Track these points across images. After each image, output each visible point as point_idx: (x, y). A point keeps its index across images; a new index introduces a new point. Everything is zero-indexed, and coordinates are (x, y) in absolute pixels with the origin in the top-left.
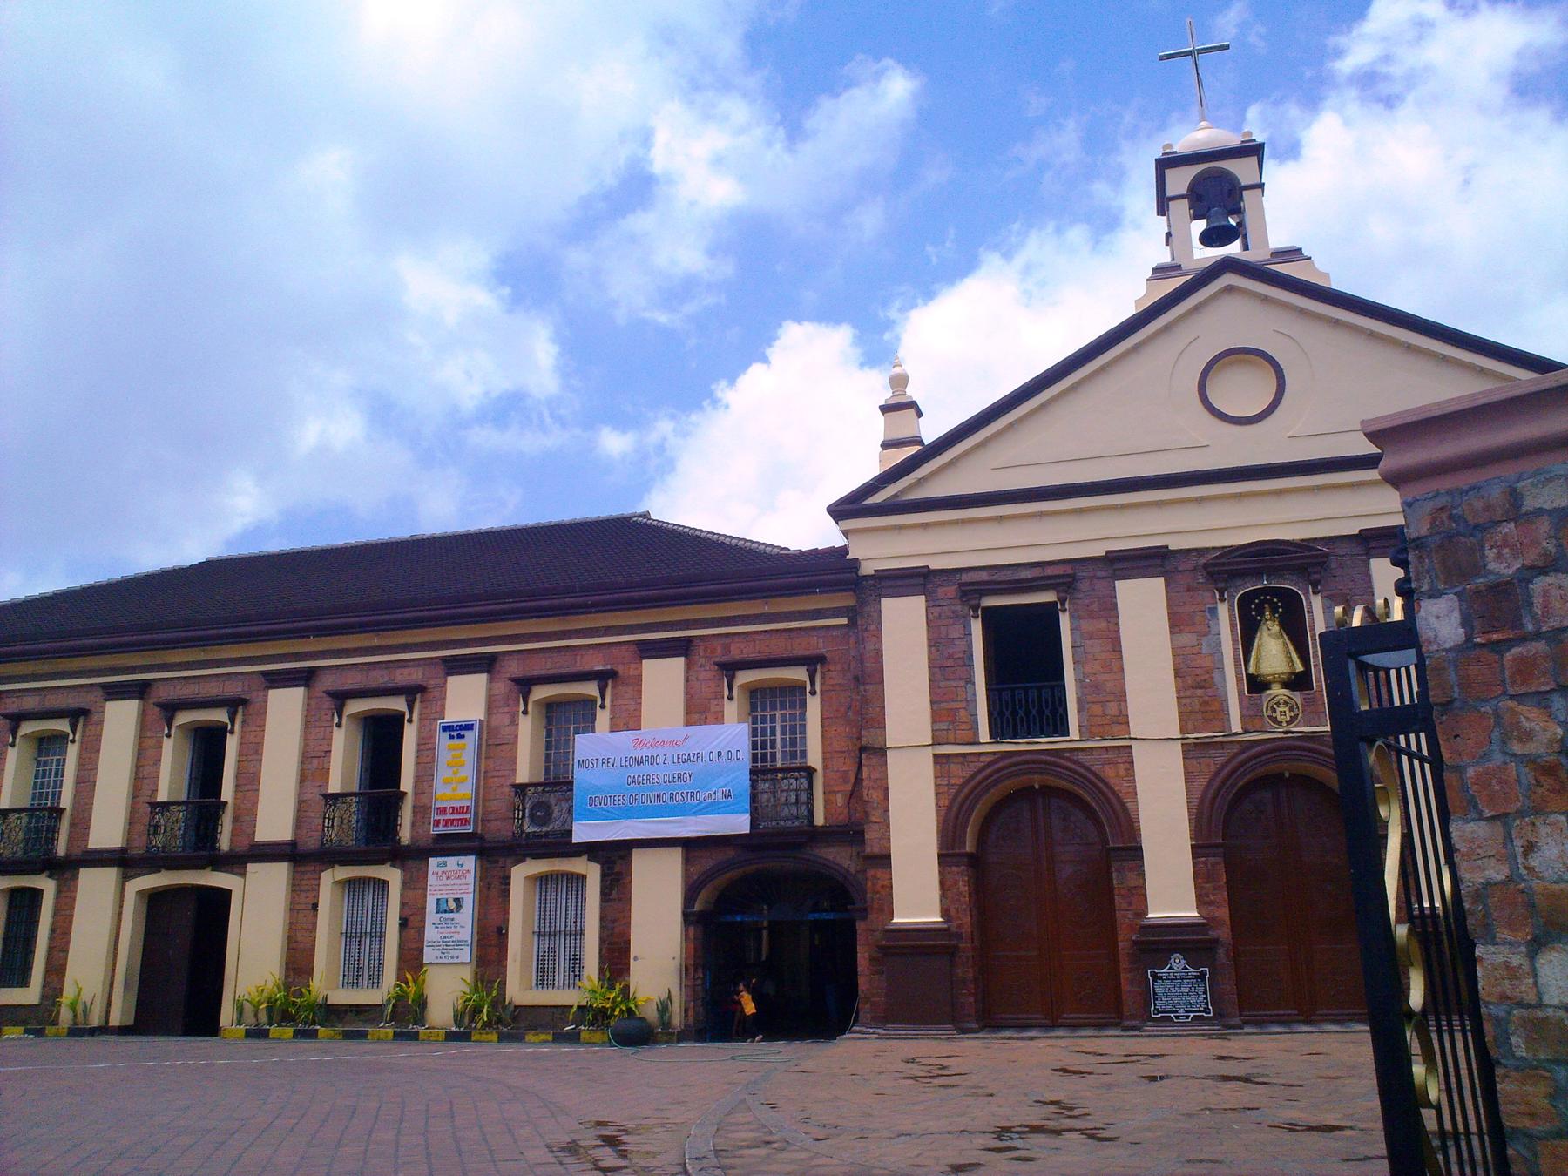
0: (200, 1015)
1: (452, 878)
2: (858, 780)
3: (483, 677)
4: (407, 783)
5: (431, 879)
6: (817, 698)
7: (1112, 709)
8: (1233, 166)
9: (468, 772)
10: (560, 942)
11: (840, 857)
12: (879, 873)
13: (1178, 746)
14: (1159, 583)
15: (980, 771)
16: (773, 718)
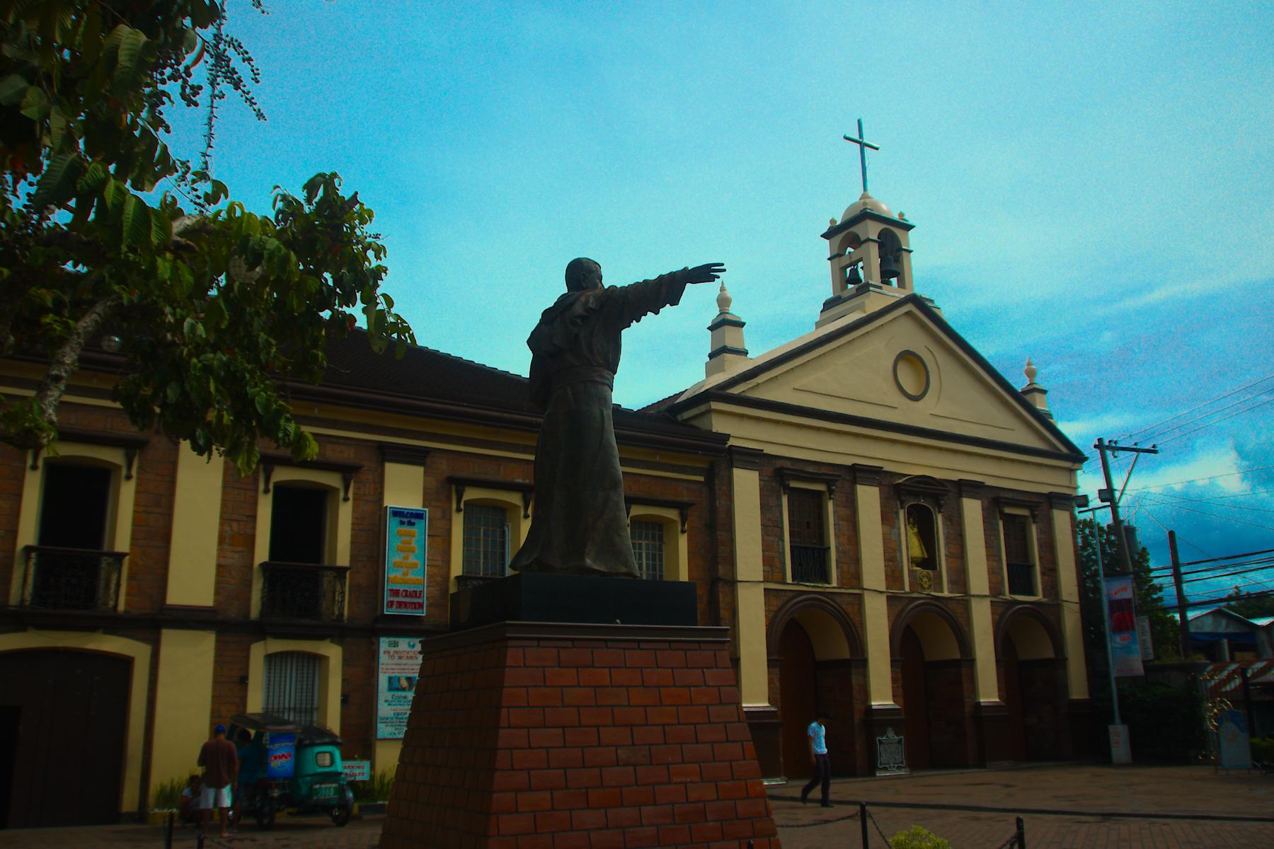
4: (122, 540)
5: (383, 658)
8: (899, 232)
13: (883, 598)
15: (787, 602)
16: (640, 545)
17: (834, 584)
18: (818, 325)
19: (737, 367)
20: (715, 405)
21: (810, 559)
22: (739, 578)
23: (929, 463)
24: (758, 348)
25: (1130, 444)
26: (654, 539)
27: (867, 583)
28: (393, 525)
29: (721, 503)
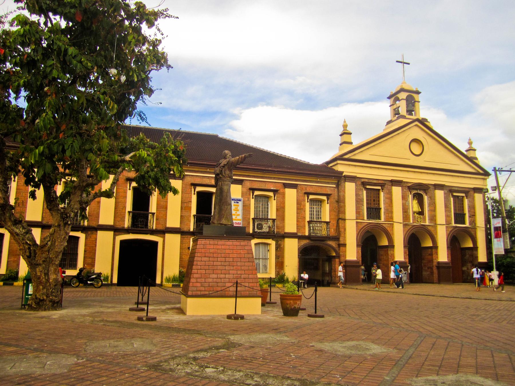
0: (328, 281)
6: (16, 183)
7: (390, 215)
8: (414, 95)
9: (240, 212)
10: (261, 261)
11: (333, 244)
12: (343, 248)
13: (445, 226)
16: (314, 208)
18: (384, 130)
19: (349, 148)
20: (339, 162)
21: (374, 211)
22: (347, 218)
23: (437, 179)
24: (356, 141)
25: (508, 169)
26: (318, 205)
27: (395, 220)
29: (341, 194)
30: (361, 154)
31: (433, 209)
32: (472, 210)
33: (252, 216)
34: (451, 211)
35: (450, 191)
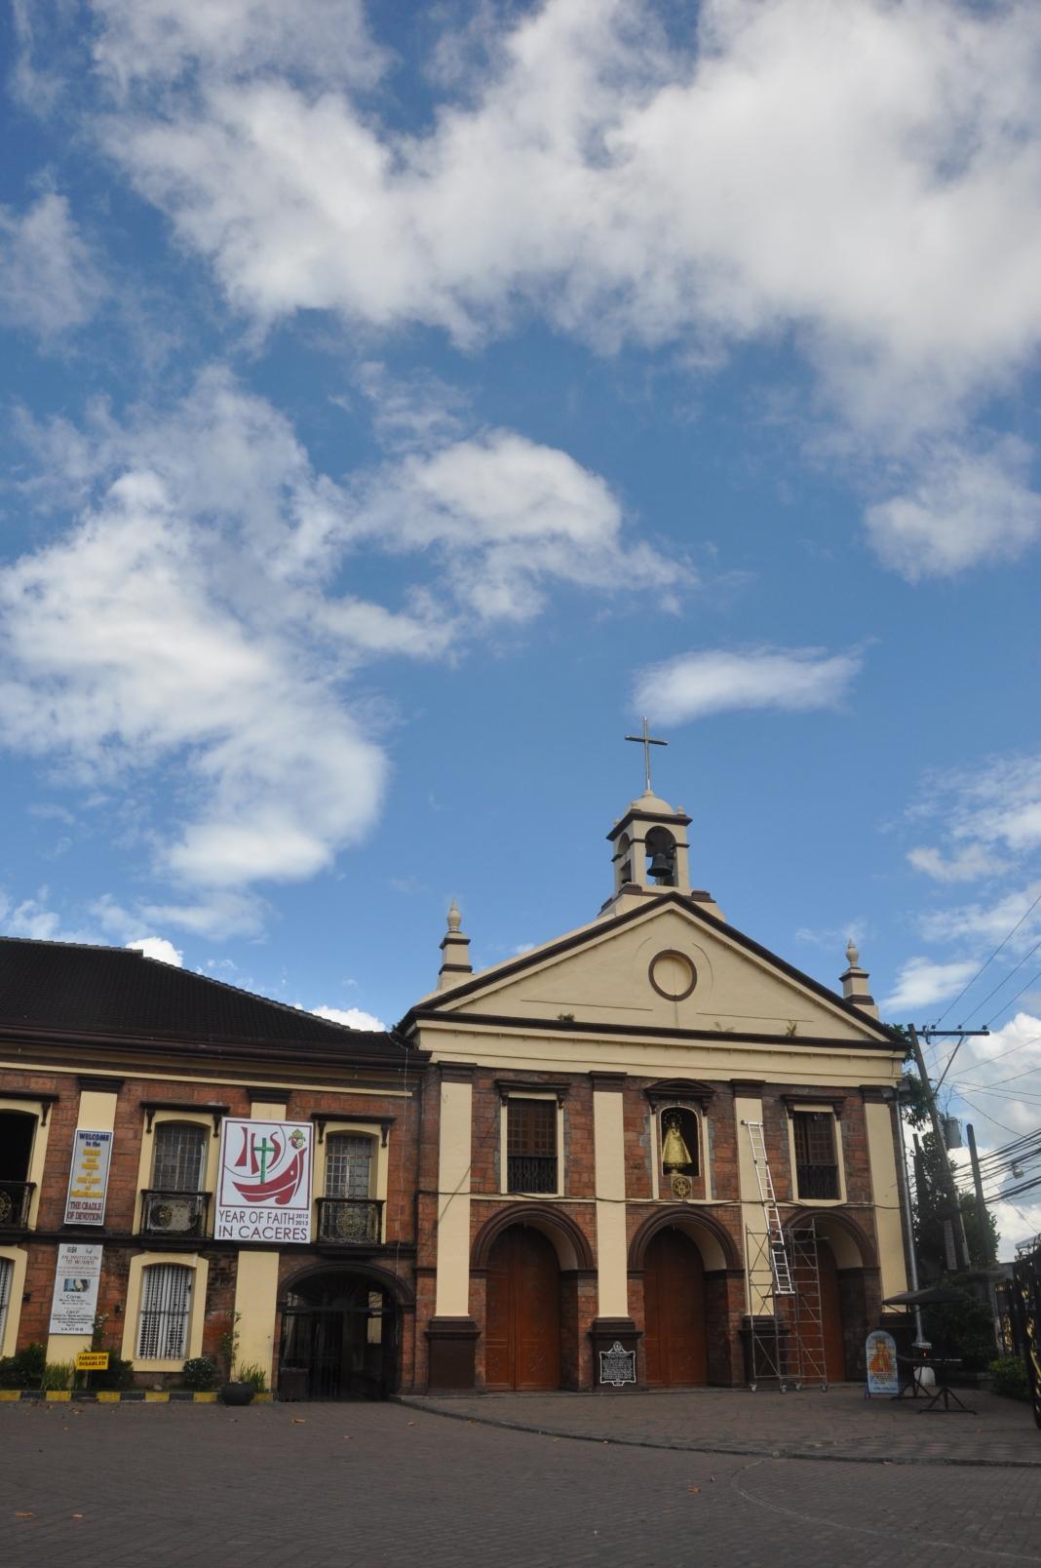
1: (79, 1262)
2: (415, 1214)
3: (114, 1096)
4: (36, 1173)
7: (585, 1177)
8: (672, 828)
9: (103, 1171)
11: (400, 1268)
14: (619, 1096)
17: (561, 1192)
19: (463, 980)
20: (420, 1023)
21: (533, 1165)
23: (746, 1066)
27: (746, 1193)
28: (79, 1146)
29: (428, 1117)
30: (492, 999)
31: (729, 1154)
32: (859, 1155)
33: (144, 1181)
34: (788, 1161)
35: (782, 1099)
